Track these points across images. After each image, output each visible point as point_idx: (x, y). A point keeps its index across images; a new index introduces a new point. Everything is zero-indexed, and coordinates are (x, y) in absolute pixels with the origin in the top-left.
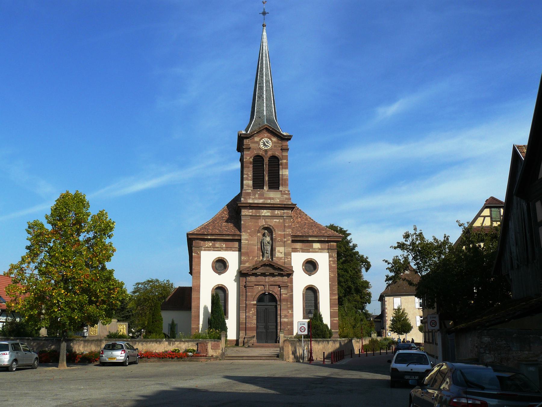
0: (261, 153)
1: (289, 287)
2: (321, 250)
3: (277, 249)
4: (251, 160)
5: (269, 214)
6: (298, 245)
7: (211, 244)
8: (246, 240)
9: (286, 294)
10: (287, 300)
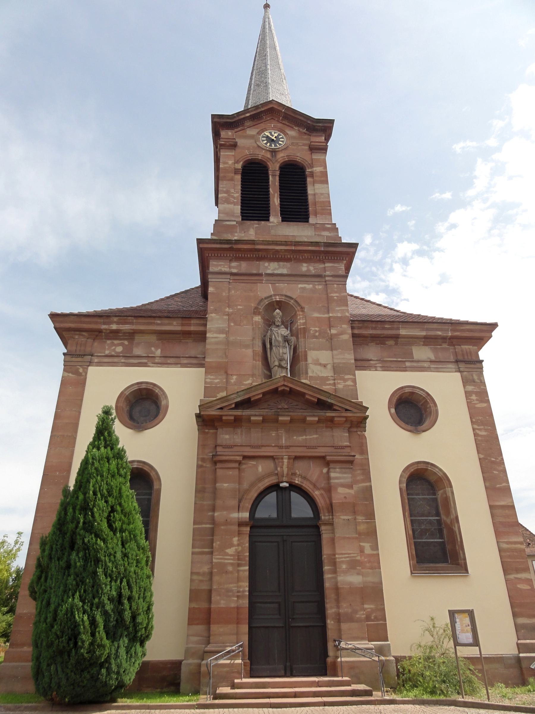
0: (261, 155)
1: (355, 460)
2: (437, 364)
3: (312, 355)
4: (239, 166)
5: (285, 271)
6: (372, 352)
7: (119, 349)
8: (220, 331)
9: (350, 487)
10: (354, 505)
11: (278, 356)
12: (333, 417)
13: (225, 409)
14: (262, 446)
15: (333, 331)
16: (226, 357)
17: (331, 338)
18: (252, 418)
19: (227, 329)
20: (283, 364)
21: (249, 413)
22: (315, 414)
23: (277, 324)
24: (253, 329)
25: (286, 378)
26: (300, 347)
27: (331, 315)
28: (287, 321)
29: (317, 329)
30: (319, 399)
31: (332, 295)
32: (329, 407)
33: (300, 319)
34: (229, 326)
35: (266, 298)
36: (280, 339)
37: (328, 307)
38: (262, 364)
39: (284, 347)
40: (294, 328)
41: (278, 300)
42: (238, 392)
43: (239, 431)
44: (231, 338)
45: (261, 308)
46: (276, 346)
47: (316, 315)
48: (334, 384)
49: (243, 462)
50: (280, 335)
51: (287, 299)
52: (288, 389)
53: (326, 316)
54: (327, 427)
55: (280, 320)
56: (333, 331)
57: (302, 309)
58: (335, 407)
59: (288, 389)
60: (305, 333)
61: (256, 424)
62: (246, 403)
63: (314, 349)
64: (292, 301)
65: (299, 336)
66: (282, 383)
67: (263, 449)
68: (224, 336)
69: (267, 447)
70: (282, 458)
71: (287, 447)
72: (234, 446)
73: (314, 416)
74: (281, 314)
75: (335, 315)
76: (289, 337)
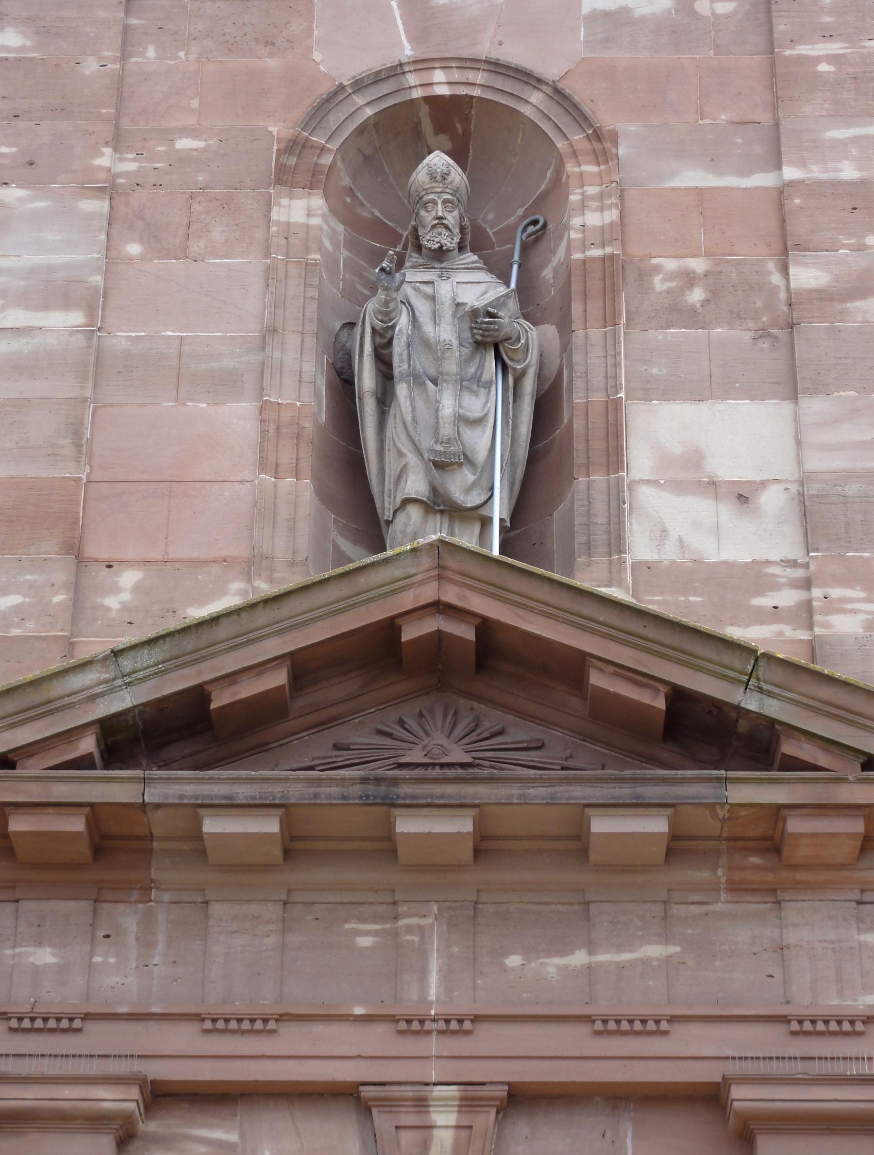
3: (657, 431)
11: (426, 442)
12: (778, 811)
13: (32, 768)
14: (281, 1018)
15: (806, 276)
16: (82, 448)
17: (789, 319)
18: (211, 825)
19: (98, 279)
20: (460, 487)
21: (189, 789)
22: (651, 792)
23: (431, 240)
24: (269, 274)
25: (450, 562)
26: (579, 383)
27: (790, 173)
28: (507, 235)
29: (698, 265)
30: (678, 697)
31: (803, 50)
32: (755, 745)
33: (583, 207)
34: (111, 258)
35: (359, 85)
36: (446, 332)
37: (777, 125)
38: (323, 494)
39: (471, 383)
40: (547, 273)
41: (443, 91)
42: (116, 654)
43: (128, 919)
44: (121, 337)
45: (330, 143)
46: (416, 379)
47: (693, 177)
48: (806, 614)
49: (151, 1127)
50: (447, 310)
51: (499, 82)
52: (466, 632)
53: (763, 180)
54: (737, 888)
55: (451, 219)
56: (806, 276)
57: (601, 142)
58: (789, 748)
59: (466, 632)
60: (610, 293)
61: (241, 867)
62: (174, 729)
63: (671, 391)
64: (536, 98)
65: (576, 309)
66: (428, 593)
67: (291, 1040)
68: (76, 318)
69: (318, 1028)
70: (421, 1104)
71: (456, 1025)
72: (87, 1017)
73: (639, 805)
74: (457, 176)
75: (817, 173)
76: (510, 319)
